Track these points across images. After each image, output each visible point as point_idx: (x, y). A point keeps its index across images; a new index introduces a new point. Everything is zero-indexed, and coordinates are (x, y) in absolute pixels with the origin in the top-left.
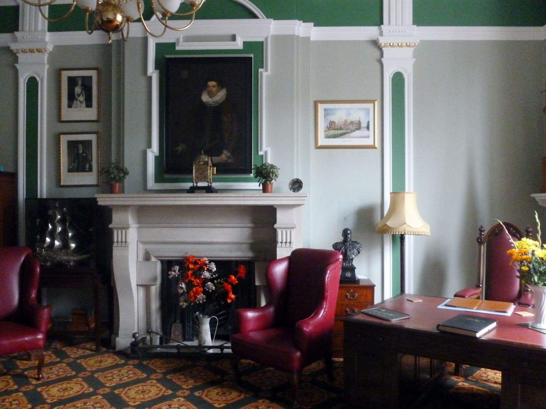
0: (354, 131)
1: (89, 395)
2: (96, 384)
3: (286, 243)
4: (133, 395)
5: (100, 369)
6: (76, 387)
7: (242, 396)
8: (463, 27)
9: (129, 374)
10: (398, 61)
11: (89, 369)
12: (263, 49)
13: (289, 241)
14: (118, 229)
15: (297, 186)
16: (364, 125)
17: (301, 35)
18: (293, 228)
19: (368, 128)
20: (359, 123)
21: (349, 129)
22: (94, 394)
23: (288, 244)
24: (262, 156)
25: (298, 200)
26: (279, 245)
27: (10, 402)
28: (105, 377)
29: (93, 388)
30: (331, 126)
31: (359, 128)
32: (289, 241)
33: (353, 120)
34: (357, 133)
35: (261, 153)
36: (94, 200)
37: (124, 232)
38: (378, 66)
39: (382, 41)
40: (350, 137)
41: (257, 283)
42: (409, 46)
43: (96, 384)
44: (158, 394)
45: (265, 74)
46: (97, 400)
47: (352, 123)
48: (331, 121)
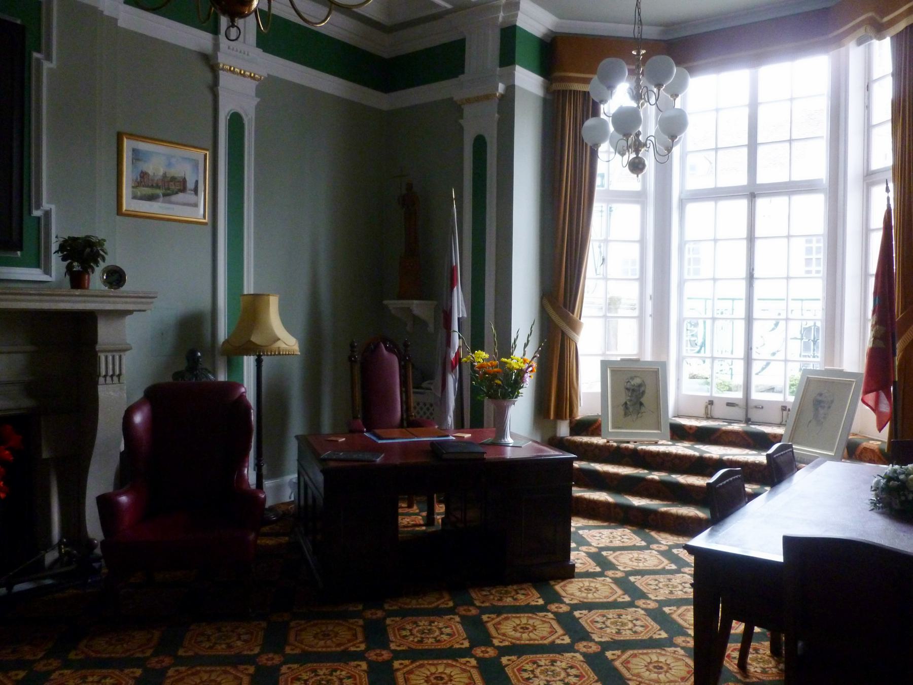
0: (177, 193)
3: (112, 376)
7: (157, 634)
8: (295, 64)
10: (237, 96)
12: (39, 20)
13: (117, 372)
14: (102, 351)
15: (115, 277)
16: (190, 185)
17: (106, 13)
18: (125, 350)
19: (196, 191)
20: (184, 181)
21: (169, 189)
23: (115, 379)
24: (39, 218)
25: (142, 303)
26: (101, 380)
30: (143, 179)
31: (183, 190)
32: (117, 372)
33: (176, 175)
34: (180, 197)
35: (36, 213)
37: (117, 358)
38: (209, 98)
39: (223, 59)
40: (171, 203)
41: (45, 455)
42: (254, 78)
45: (46, 65)
46: (571, 663)
47: (173, 179)
48: (142, 172)
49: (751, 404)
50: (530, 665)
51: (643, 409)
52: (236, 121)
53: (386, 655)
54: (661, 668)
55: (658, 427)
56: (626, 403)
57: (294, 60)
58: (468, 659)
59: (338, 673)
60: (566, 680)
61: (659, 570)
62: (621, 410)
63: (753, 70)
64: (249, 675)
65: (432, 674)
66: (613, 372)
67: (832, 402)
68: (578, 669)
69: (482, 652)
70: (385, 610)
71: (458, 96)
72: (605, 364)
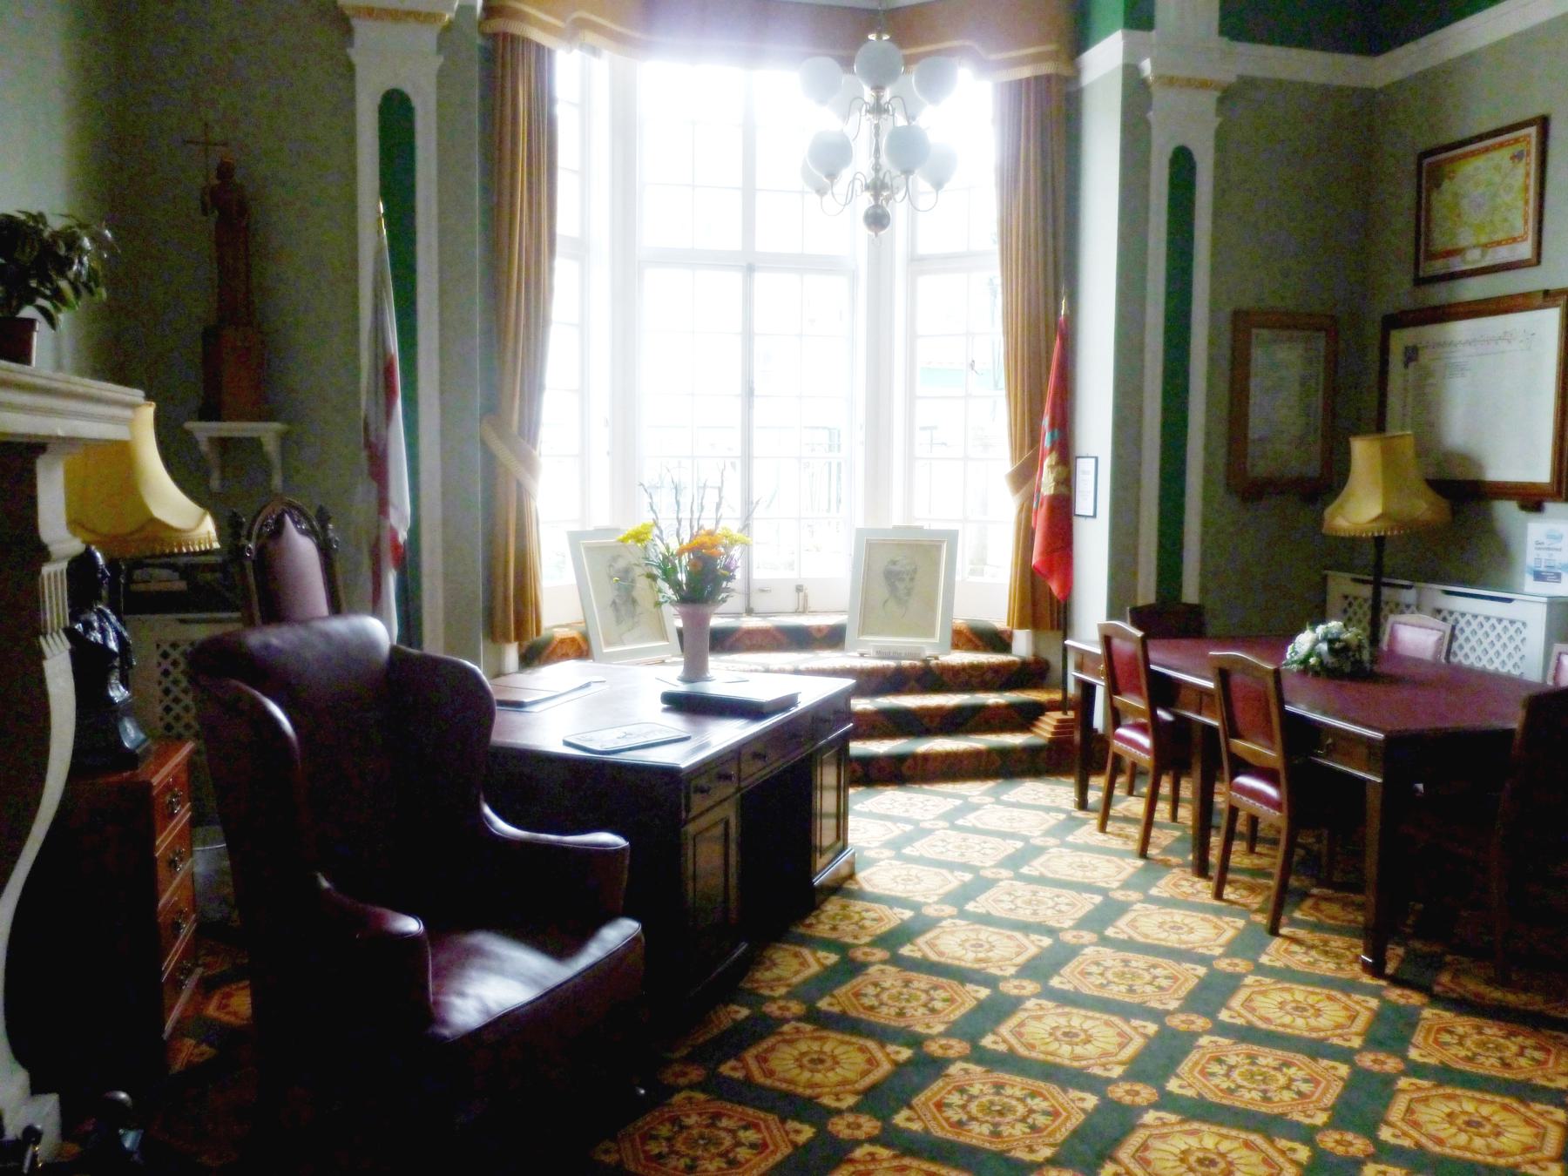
14: (1419, 594)
49: (755, 586)
51: (639, 610)
52: (396, 112)
55: (664, 637)
56: (614, 603)
60: (731, 1155)
62: (610, 612)
66: (589, 549)
67: (915, 571)
70: (1405, 1058)
72: (575, 538)
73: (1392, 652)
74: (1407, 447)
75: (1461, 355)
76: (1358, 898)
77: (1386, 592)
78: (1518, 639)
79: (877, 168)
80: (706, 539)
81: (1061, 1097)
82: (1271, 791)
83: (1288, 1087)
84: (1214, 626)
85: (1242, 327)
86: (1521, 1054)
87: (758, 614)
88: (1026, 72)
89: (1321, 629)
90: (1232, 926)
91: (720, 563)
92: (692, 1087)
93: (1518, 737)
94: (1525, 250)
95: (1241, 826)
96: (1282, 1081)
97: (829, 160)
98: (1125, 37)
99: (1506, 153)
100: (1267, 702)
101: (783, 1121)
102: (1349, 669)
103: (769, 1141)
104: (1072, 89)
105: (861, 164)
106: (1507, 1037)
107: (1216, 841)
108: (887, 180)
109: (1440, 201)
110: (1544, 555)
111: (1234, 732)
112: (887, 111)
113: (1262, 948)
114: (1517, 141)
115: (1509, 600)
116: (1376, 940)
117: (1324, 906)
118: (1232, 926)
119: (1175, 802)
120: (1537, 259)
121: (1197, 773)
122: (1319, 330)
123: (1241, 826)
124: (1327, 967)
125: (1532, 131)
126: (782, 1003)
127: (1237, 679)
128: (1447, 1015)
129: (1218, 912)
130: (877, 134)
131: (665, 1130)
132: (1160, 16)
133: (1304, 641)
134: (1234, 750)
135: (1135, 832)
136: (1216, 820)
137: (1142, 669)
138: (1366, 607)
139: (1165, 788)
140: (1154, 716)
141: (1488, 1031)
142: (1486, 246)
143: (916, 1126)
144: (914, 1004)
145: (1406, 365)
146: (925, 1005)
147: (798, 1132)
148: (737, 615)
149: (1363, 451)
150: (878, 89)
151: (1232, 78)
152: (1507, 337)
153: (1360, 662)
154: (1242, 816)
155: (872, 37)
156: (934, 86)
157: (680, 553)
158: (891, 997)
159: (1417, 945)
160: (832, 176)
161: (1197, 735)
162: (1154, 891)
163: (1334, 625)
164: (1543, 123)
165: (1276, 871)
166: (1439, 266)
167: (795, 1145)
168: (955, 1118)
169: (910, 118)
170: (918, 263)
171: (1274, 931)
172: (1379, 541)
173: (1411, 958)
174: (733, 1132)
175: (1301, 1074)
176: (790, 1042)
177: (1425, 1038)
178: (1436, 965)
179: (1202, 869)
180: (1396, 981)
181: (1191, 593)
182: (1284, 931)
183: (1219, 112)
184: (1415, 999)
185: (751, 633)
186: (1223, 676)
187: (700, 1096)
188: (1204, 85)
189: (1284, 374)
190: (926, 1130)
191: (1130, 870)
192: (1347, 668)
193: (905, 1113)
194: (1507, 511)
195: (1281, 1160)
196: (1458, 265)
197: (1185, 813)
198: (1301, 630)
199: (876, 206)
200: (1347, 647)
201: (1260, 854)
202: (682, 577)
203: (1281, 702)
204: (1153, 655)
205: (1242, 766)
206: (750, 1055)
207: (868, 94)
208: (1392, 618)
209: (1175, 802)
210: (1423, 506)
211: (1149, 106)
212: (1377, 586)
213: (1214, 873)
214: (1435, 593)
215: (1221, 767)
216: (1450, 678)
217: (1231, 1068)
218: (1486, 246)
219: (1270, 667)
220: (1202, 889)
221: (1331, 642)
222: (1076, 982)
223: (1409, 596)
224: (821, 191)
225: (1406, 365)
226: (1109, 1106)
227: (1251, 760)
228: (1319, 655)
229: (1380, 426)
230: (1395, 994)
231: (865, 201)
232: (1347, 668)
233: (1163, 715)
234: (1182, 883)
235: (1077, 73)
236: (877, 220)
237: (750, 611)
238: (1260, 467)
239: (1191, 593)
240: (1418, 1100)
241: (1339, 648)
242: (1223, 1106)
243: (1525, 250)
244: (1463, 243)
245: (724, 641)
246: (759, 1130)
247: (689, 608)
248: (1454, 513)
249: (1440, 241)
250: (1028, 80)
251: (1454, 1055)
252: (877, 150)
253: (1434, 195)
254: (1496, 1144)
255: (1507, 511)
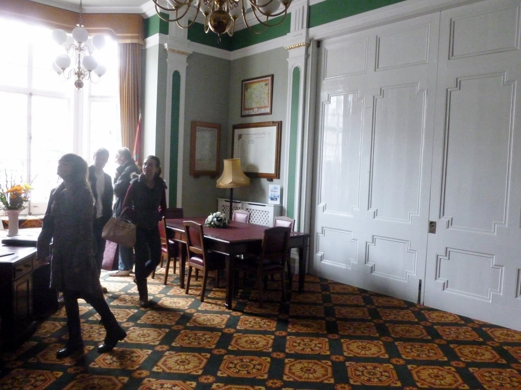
1: (427, 341)
2: (393, 352)
4: (425, 375)
5: (440, 323)
6: (374, 349)
9: (429, 352)
11: (430, 321)
22: (388, 361)
27: (254, 365)
28: (405, 348)
29: (389, 355)
36: (167, 188)
43: (393, 352)
44: (492, 359)
46: (387, 369)
50: (362, 367)
53: (341, 358)
54: (184, 362)
57: (351, 15)
58: (327, 361)
59: (254, 362)
61: (454, 323)
63: (329, 54)
64: (207, 358)
65: (305, 367)
68: (484, 379)
69: (396, 361)
71: (287, 46)
73: (235, 222)
74: (239, 162)
75: (253, 137)
76: (224, 290)
77: (234, 204)
78: (267, 216)
79: (79, 68)
80: (18, 188)
81: (141, 352)
82: (201, 261)
83: (205, 340)
84: (185, 214)
85: (193, 126)
86: (265, 324)
87: (33, 215)
88: (128, 41)
89: (214, 214)
90: (190, 301)
91: (23, 195)
92: (19, 367)
93: (263, 241)
94: (268, 110)
95: (193, 273)
96: (204, 339)
97: (63, 65)
98: (159, 35)
99: (264, 83)
100: (199, 235)
101: (52, 372)
102: (221, 225)
103: (48, 378)
104: (143, 48)
105: (73, 66)
106: (261, 320)
107: (186, 278)
108: (83, 72)
109: (247, 94)
110: (273, 193)
111: (190, 244)
112: (83, 50)
113: (199, 306)
114: (266, 80)
115: (265, 206)
116: (229, 300)
117: (216, 293)
118: (190, 301)
119: (175, 268)
120: (271, 113)
121: (181, 261)
122: (215, 128)
123: (193, 273)
124: (216, 308)
125: (270, 78)
126: (49, 339)
127: (191, 229)
128: (247, 317)
129: (187, 297)
130: (79, 57)
131: (10, 382)
132: (170, 32)
133: (210, 218)
134: (190, 249)
135: (163, 278)
136: (186, 273)
137: (164, 228)
138: (229, 208)
139: (172, 264)
140: (168, 243)
141: (257, 319)
142: (259, 108)
143: (97, 366)
144: (94, 333)
145: (239, 140)
146: (98, 333)
147: (57, 374)
148: (26, 215)
149: (227, 163)
150: (80, 43)
151: (191, 53)
152: (264, 133)
153: (225, 223)
154: (193, 269)
155: (78, 25)
156: (98, 42)
157: (7, 193)
158: (87, 332)
159: (241, 300)
160: (64, 69)
161: (180, 246)
162: (168, 294)
163: (218, 213)
164: (272, 76)
165: (202, 285)
166: (247, 113)
167: (57, 378)
168: (109, 362)
169: (90, 53)
170: (91, 97)
171: (202, 301)
172: (232, 189)
173: (239, 303)
174: (35, 378)
175: (208, 336)
176: (52, 350)
177: (266, 364)
178: (245, 305)
179: (182, 287)
180: (235, 310)
181: (179, 205)
182: (205, 301)
183: (187, 62)
184: (239, 314)
185: (31, 221)
186: (187, 228)
187: (21, 370)
188: (183, 53)
189: (206, 140)
190: (100, 367)
191: (162, 288)
192: (222, 225)
193: (93, 363)
194: (264, 181)
195: (202, 358)
196: (252, 112)
197: (178, 271)
198: (210, 215)
199: (79, 80)
200: (221, 220)
201: (199, 281)
202: (8, 201)
203: (203, 235)
204: (167, 224)
205: (193, 254)
206: (39, 355)
207: (76, 43)
208: (235, 211)
209: (175, 268)
210: (243, 180)
211: (167, 58)
212: (231, 202)
213: (186, 287)
214: (246, 205)
215: (187, 256)
216: (248, 226)
217: (190, 338)
218: (259, 108)
219: (200, 225)
220: (183, 292)
221: (217, 218)
222: (145, 321)
223: (240, 205)
224: (59, 73)
225: (239, 140)
226: (155, 352)
227: (195, 252)
228: (214, 222)
229: (232, 157)
230: (234, 313)
231: (75, 78)
232: (222, 225)
233: (171, 242)
234: (177, 290)
235: (145, 43)
236: (79, 85)
237: (30, 214)
238: (198, 168)
239: (179, 205)
240: (239, 338)
241: (219, 220)
242: (188, 347)
243: (268, 110)
244: (253, 107)
245: (24, 224)
246: (44, 376)
247: (11, 211)
248: (251, 181)
249: (248, 105)
250: (129, 44)
251: (248, 326)
252: (79, 62)
253: (246, 93)
254: (257, 346)
255: (264, 181)
